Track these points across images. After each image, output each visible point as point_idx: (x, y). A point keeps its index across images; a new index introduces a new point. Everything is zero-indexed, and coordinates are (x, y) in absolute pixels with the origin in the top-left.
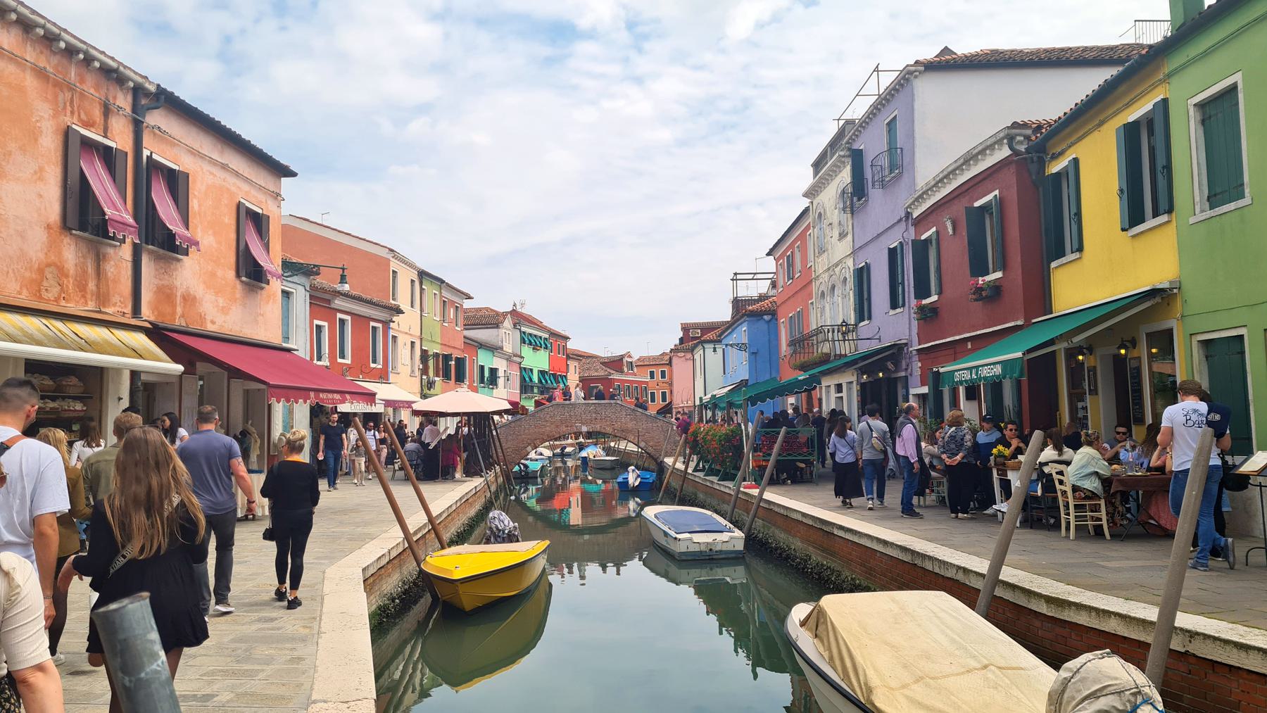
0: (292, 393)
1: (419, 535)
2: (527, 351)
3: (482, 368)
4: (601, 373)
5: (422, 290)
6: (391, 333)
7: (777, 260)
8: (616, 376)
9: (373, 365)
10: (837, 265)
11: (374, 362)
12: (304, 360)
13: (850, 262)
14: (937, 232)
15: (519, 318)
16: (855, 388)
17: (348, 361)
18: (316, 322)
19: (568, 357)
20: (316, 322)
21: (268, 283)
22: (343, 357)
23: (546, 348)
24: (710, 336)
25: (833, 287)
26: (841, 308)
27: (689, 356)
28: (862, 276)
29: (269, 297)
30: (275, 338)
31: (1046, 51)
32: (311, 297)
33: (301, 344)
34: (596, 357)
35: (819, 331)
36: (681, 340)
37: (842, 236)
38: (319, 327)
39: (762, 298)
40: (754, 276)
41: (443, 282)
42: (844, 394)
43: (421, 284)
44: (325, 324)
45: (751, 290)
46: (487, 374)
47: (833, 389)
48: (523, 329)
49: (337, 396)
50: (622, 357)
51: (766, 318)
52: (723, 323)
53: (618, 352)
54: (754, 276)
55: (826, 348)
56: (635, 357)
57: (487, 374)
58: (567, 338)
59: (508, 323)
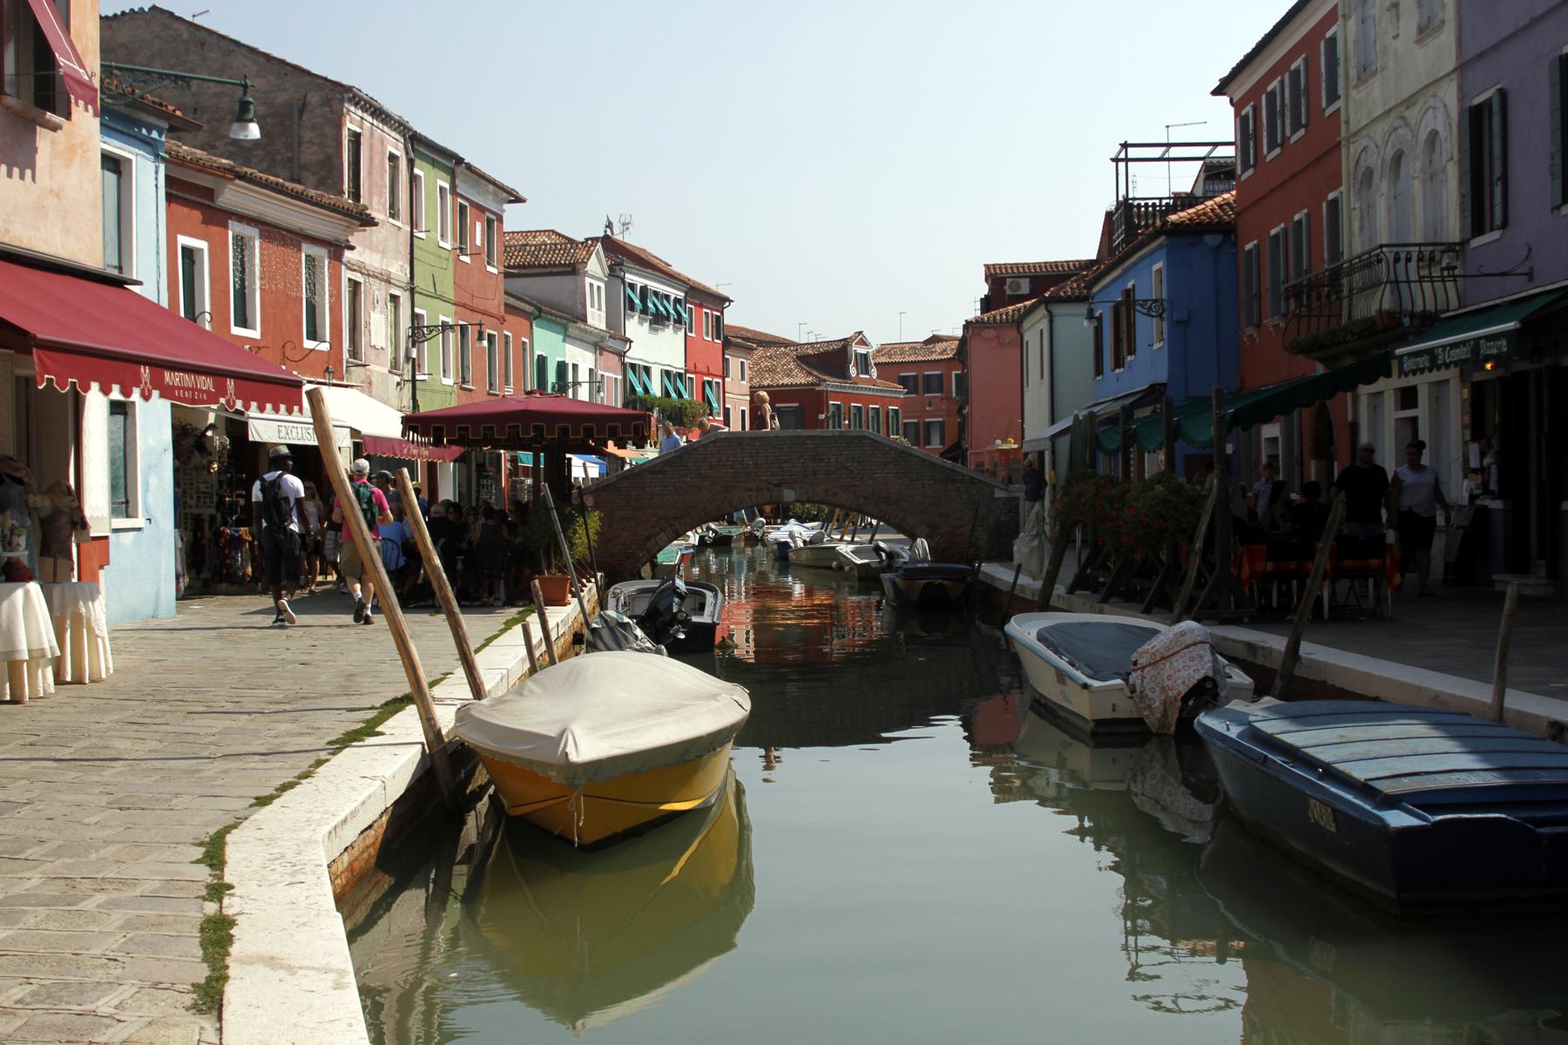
0: (118, 367)
1: (1154, 245)
2: (635, 328)
3: (542, 361)
5: (413, 179)
6: (346, 275)
7: (1237, 106)
8: (831, 383)
9: (309, 344)
10: (1410, 102)
11: (313, 335)
12: (157, 307)
13: (1449, 94)
14: (1308, 215)
15: (619, 254)
16: (1457, 396)
17: (255, 334)
18: (184, 240)
20: (184, 240)
21: (68, 116)
22: (243, 322)
23: (679, 321)
24: (1069, 288)
25: (1398, 158)
26: (1432, 203)
27: (1011, 335)
28: (1482, 129)
29: (71, 149)
30: (93, 256)
31: (1012, 266)
32: (170, 181)
33: (150, 277)
34: (786, 344)
35: (1370, 260)
36: (987, 304)
37: (1425, 31)
38: (189, 253)
39: (1182, 201)
40: (1166, 151)
41: (460, 161)
42: (1422, 411)
43: (411, 163)
44: (202, 245)
45: (1159, 183)
46: (552, 377)
47: (1389, 401)
48: (629, 278)
49: (206, 383)
50: (845, 344)
51: (1212, 240)
52: (1089, 264)
53: (829, 330)
54: (1166, 151)
55: (1382, 300)
56: (875, 340)
57: (552, 377)
58: (720, 301)
59: (596, 266)
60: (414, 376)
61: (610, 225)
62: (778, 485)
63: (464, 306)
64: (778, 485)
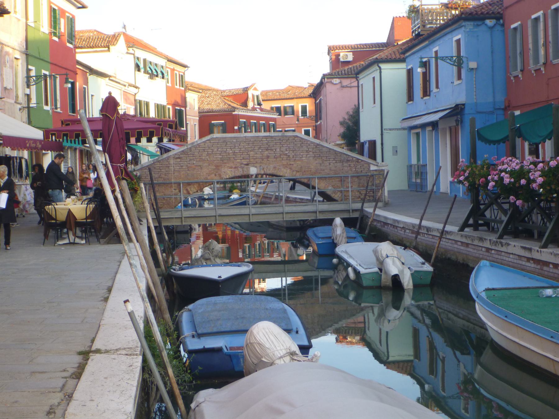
4: (222, 106)
19: (187, 89)
60: (28, 104)
61: (124, 27)
62: (247, 165)
63: (55, 65)
64: (247, 165)
